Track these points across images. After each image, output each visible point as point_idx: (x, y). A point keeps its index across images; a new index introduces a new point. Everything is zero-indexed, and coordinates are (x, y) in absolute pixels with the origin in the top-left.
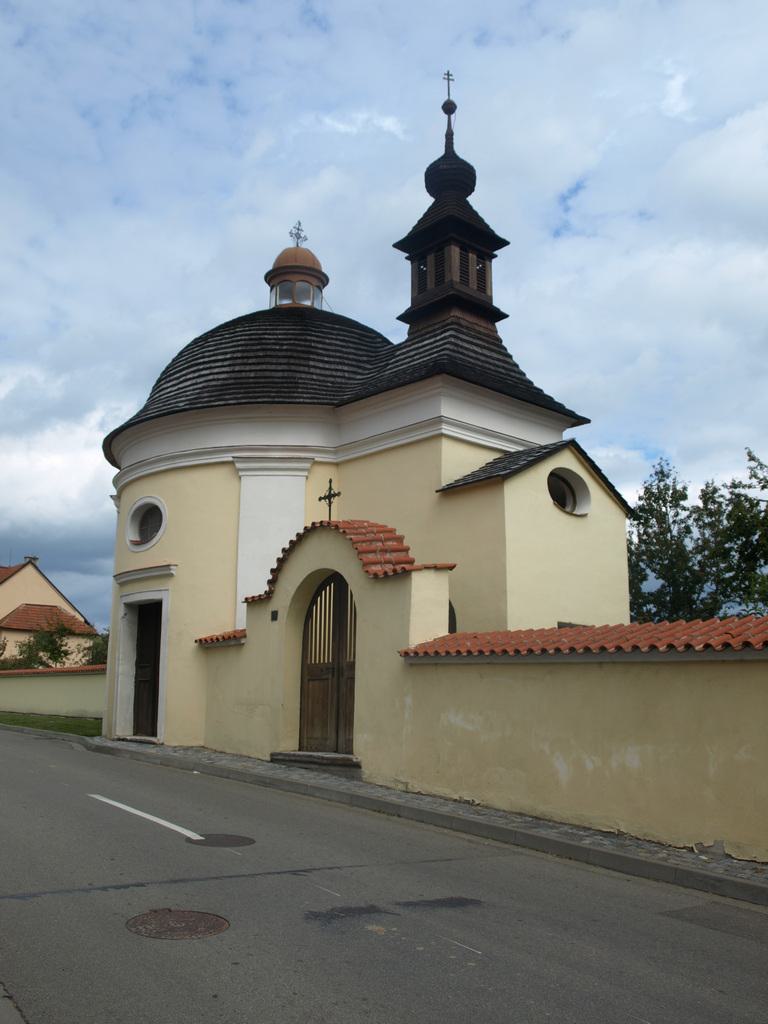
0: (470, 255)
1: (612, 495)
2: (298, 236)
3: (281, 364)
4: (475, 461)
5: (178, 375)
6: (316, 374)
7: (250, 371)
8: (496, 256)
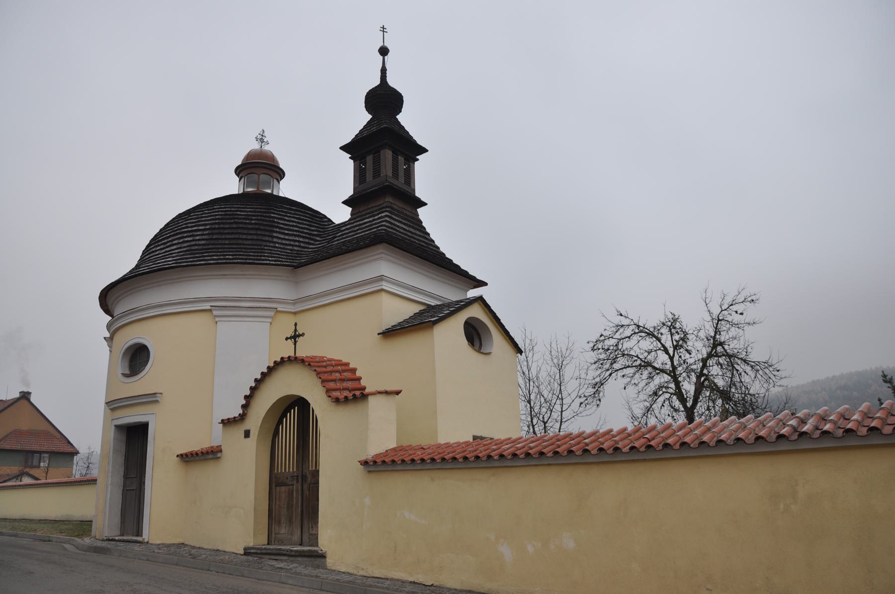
0: (400, 157)
1: (507, 338)
2: (262, 141)
3: (251, 234)
4: (408, 310)
5: (166, 241)
6: (278, 243)
7: (226, 239)
8: (418, 160)
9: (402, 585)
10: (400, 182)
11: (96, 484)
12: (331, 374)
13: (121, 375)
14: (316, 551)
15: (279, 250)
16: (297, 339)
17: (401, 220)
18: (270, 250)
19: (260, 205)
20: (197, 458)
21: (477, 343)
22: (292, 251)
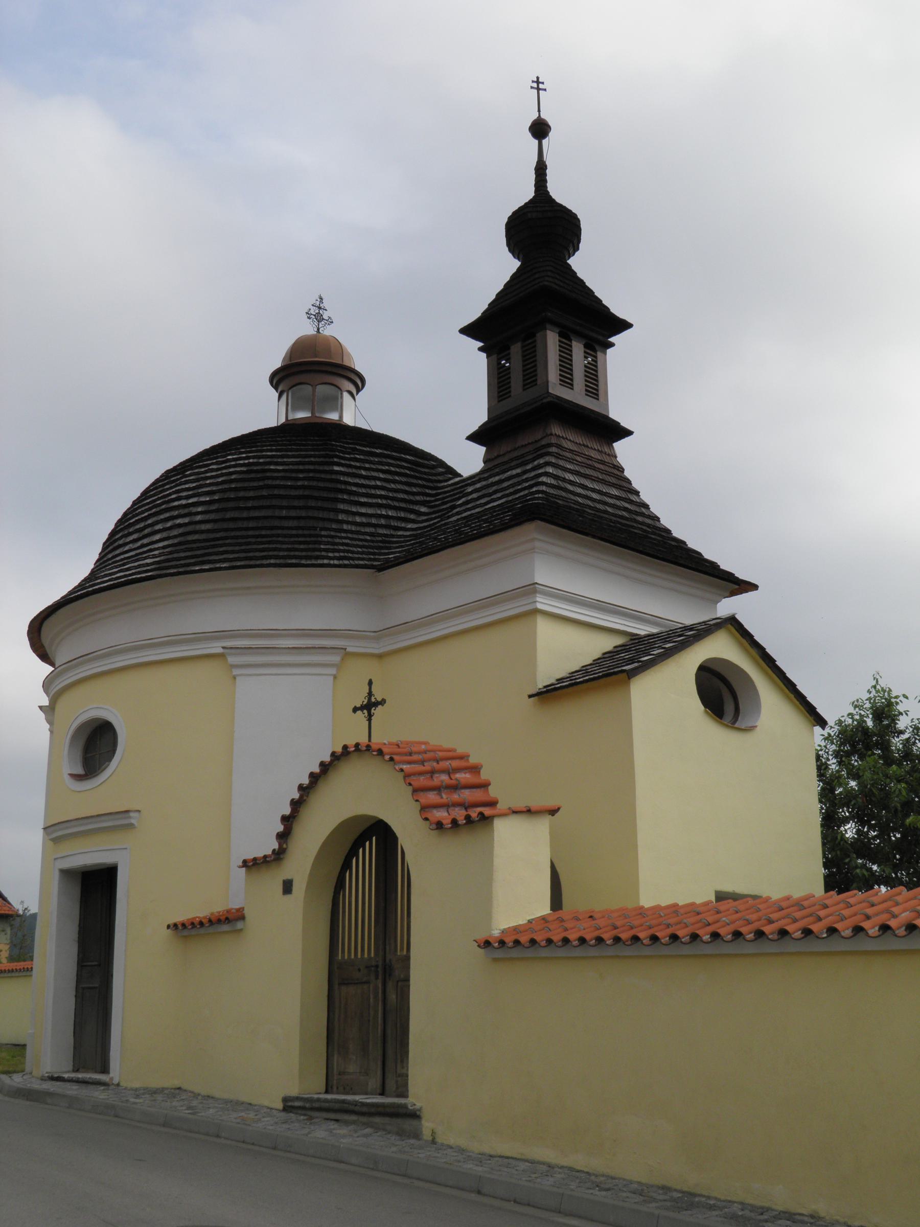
1: (792, 696)
2: (319, 318)
3: (295, 508)
5: (142, 525)
6: (348, 523)
8: (612, 345)
9: (548, 1171)
10: (577, 395)
11: (31, 976)
12: (432, 777)
13: (68, 776)
14: (405, 1106)
15: (350, 535)
16: (373, 711)
17: (577, 468)
18: (332, 537)
19: (313, 450)
20: (202, 931)
21: (729, 708)
22: (374, 536)
